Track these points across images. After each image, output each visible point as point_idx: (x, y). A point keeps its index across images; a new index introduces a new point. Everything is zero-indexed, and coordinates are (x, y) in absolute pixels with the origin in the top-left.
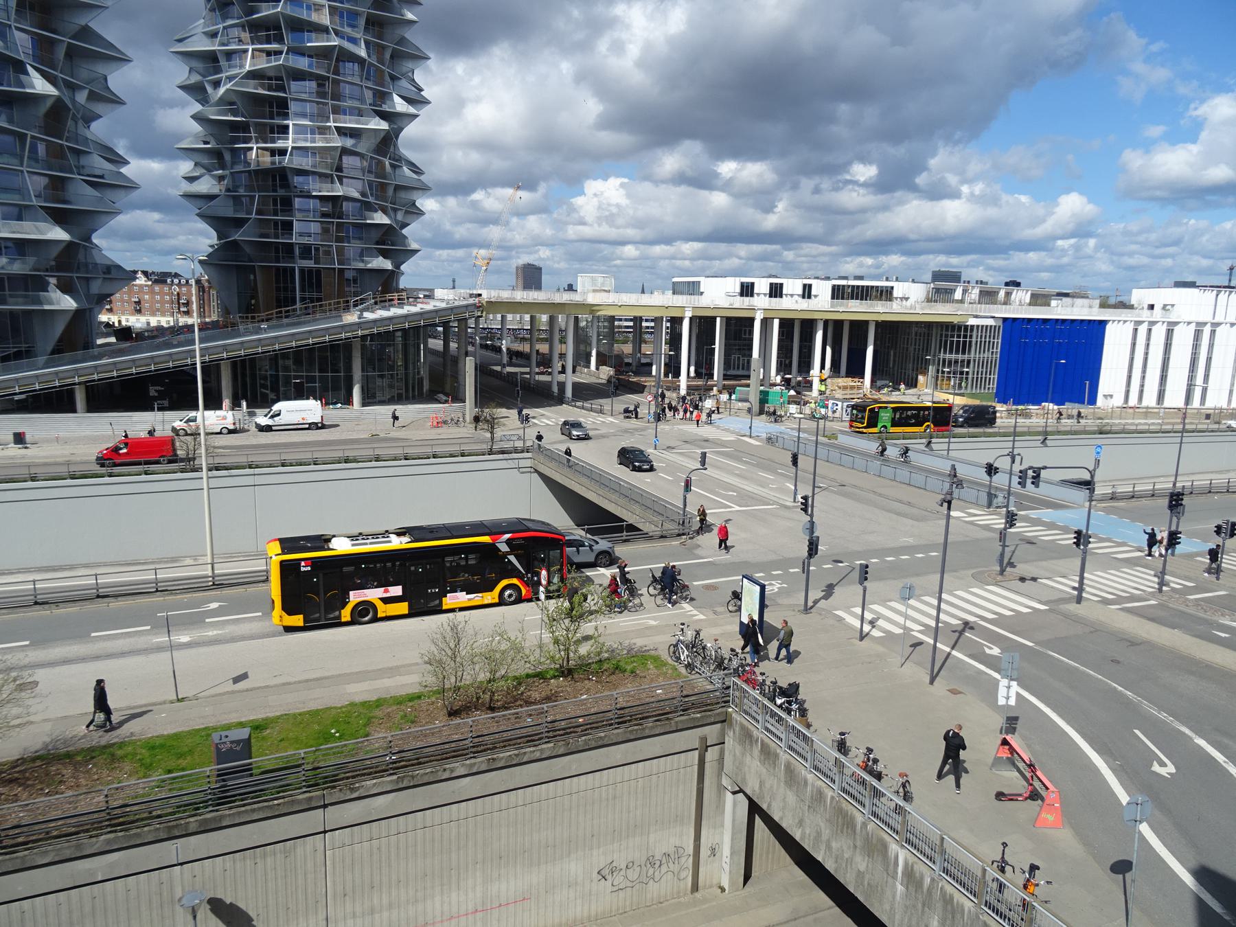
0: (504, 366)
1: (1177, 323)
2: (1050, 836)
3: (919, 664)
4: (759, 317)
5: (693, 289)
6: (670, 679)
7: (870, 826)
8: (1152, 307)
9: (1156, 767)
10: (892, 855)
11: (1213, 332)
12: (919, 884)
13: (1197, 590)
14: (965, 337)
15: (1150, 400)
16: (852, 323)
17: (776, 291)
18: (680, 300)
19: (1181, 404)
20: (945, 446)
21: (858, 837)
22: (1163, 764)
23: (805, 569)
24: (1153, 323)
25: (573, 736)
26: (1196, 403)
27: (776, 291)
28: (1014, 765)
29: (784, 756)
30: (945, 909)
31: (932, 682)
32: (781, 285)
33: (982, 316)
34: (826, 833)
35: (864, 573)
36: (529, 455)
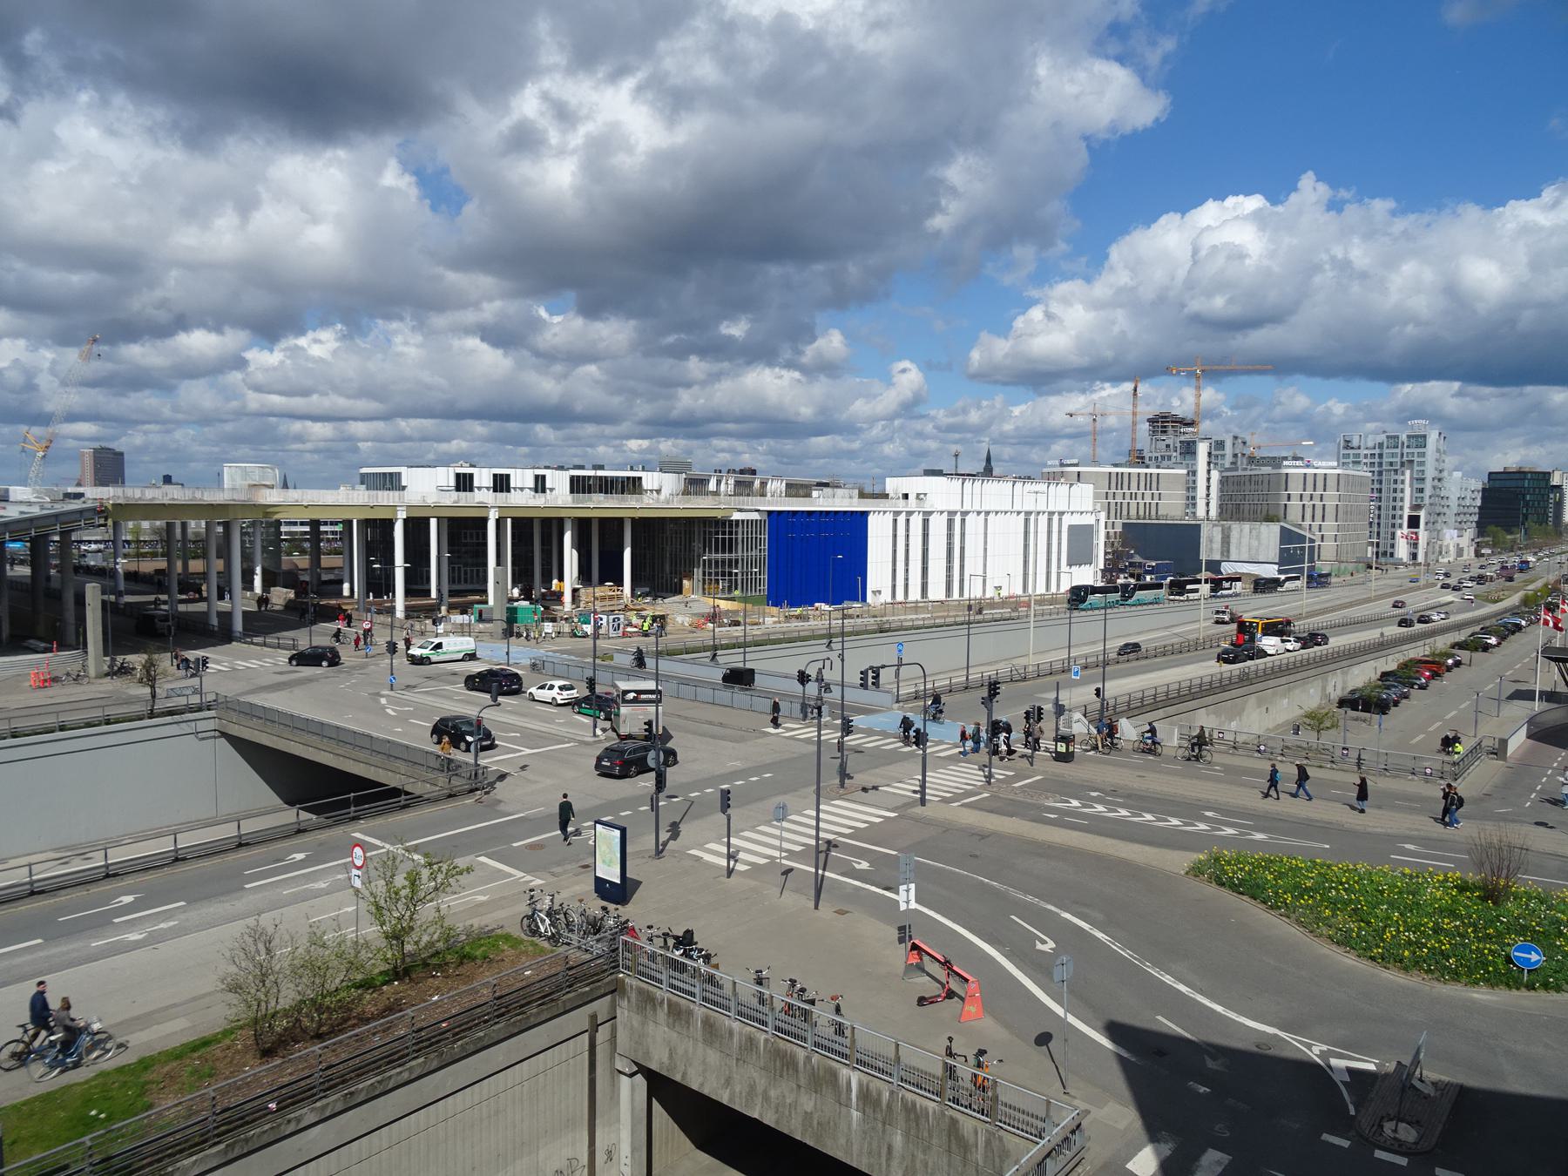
0: (120, 594)
1: (931, 513)
2: (976, 1024)
3: (796, 891)
4: (493, 516)
5: (391, 482)
6: (534, 957)
7: (815, 1058)
8: (906, 496)
9: (1039, 946)
10: (843, 1082)
11: (963, 521)
12: (876, 1103)
13: (1018, 778)
14: (731, 533)
15: (915, 594)
16: (602, 521)
17: (501, 484)
18: (385, 498)
19: (943, 598)
20: (741, 658)
21: (801, 1075)
22: (1043, 942)
23: (655, 807)
24: (910, 513)
25: (444, 1043)
26: (956, 595)
27: (501, 484)
28: (923, 970)
29: (699, 1011)
30: (908, 1120)
31: (816, 907)
32: (508, 476)
33: (747, 511)
34: (761, 1083)
35: (726, 799)
36: (212, 713)
